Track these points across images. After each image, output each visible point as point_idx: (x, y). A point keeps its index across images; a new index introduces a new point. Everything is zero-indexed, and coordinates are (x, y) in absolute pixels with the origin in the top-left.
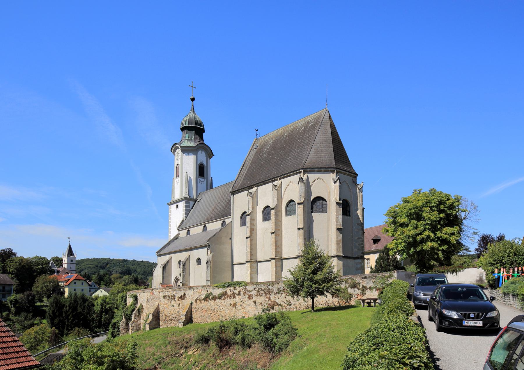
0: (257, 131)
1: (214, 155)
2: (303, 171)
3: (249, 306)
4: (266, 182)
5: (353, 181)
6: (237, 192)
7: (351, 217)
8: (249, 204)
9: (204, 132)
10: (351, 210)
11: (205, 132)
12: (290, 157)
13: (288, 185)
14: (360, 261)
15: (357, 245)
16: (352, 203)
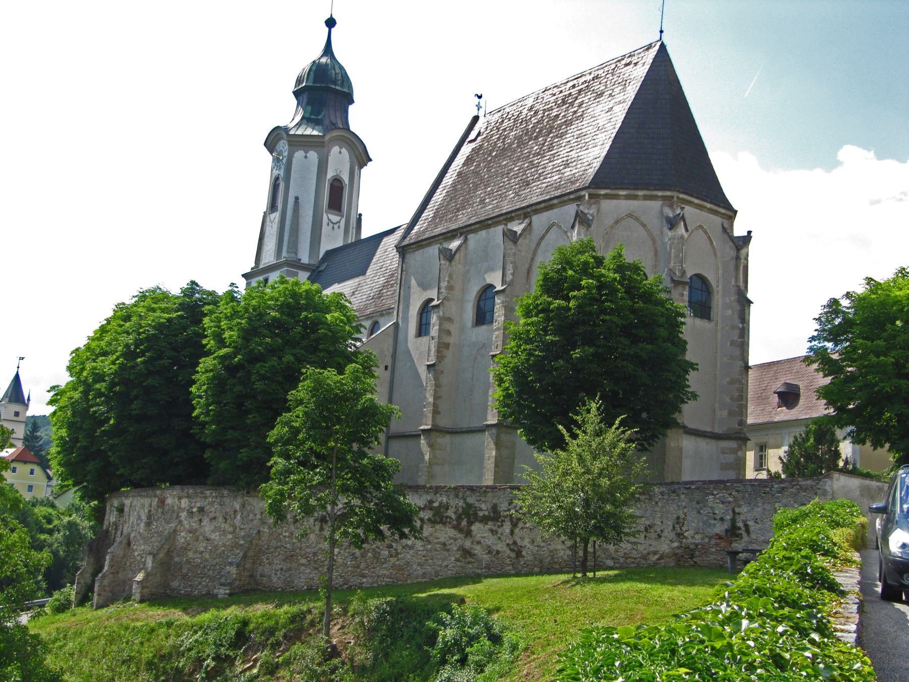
0: (480, 97)
1: (370, 160)
2: (587, 195)
3: (411, 552)
4: (490, 222)
5: (723, 227)
6: (414, 246)
7: (713, 324)
8: (442, 279)
9: (351, 101)
10: (712, 306)
11: (353, 102)
12: (557, 159)
13: (547, 231)
14: (733, 444)
15: (727, 399)
16: (718, 286)
